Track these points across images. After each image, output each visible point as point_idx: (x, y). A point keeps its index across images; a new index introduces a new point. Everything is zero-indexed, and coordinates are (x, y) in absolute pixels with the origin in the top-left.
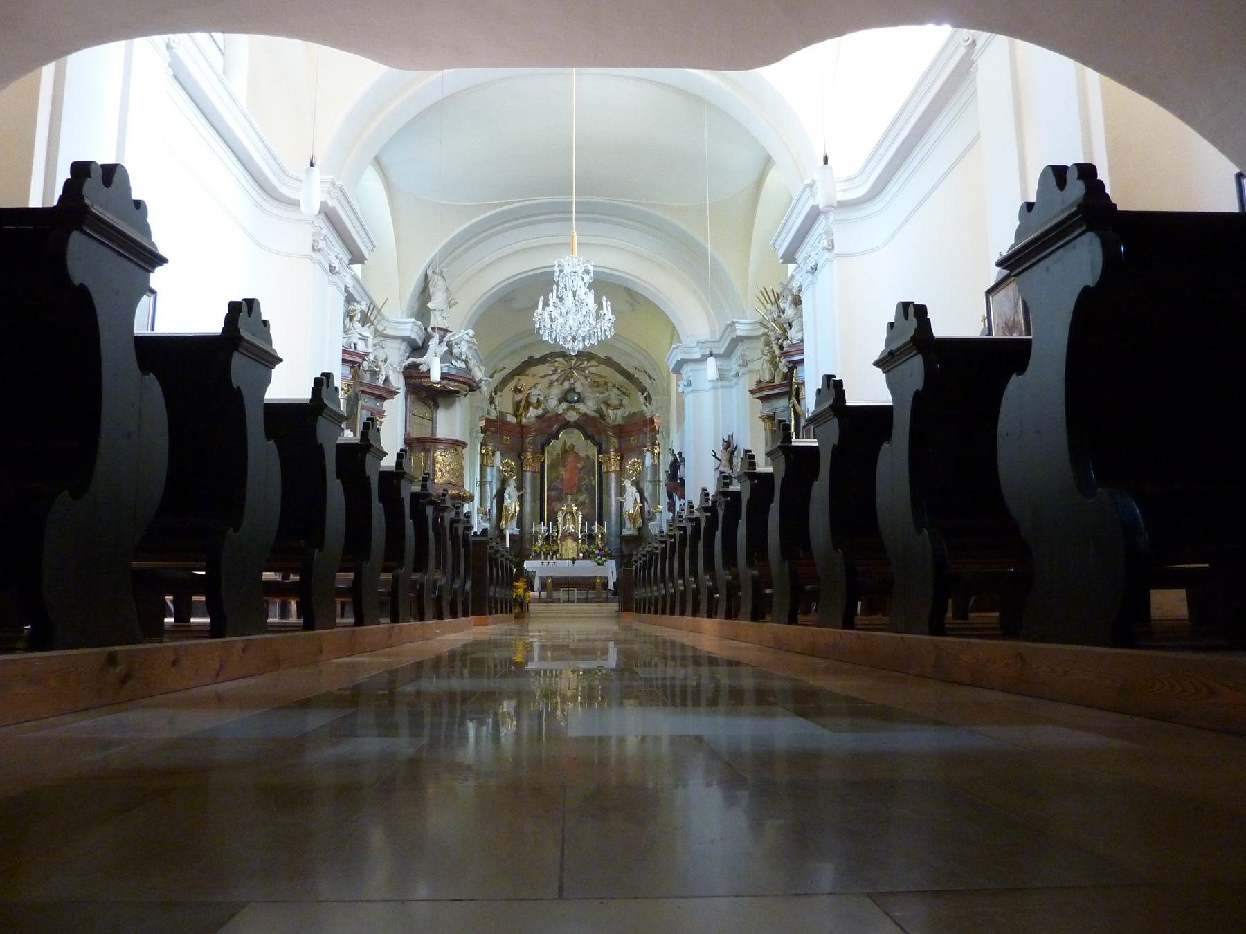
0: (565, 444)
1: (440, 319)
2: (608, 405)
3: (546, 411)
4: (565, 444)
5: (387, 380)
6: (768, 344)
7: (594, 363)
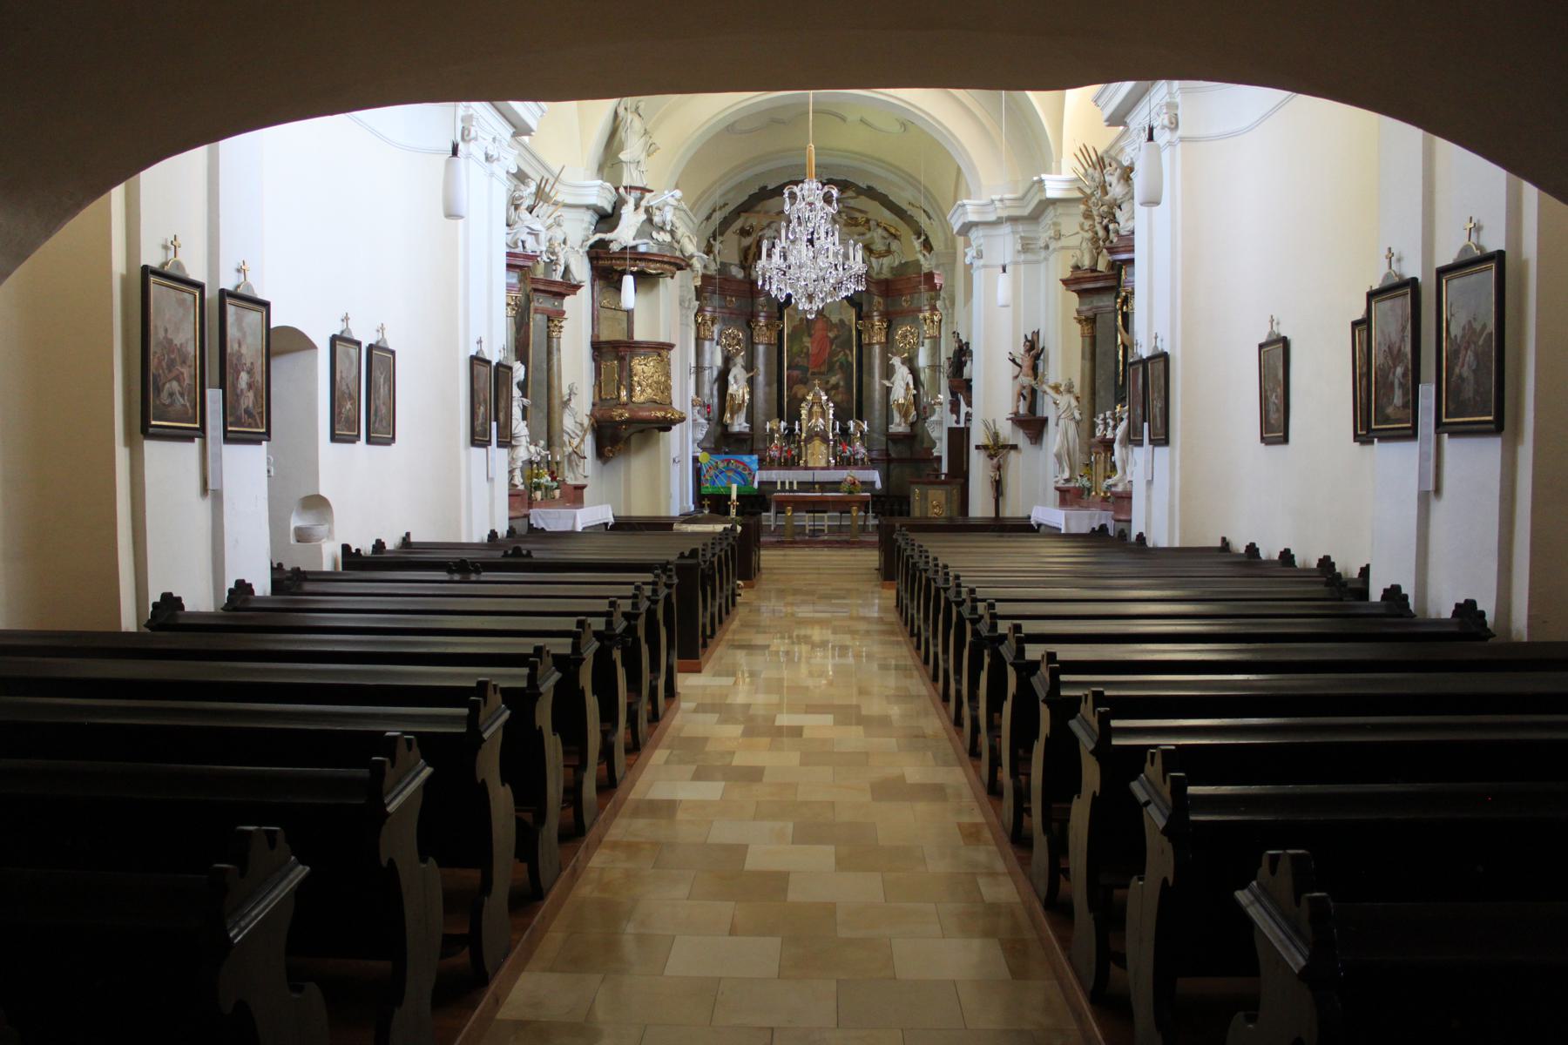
5: (567, 269)
6: (1088, 215)
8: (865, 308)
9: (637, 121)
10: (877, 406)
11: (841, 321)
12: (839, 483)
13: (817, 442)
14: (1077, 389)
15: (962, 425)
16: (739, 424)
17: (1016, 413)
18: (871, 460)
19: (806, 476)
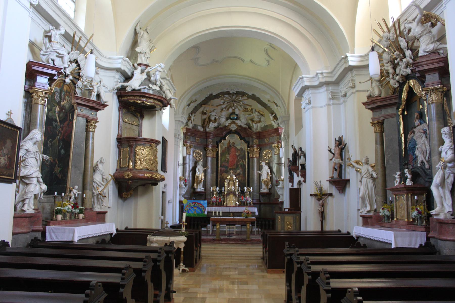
0: (229, 142)
1: (144, 58)
2: (252, 121)
3: (219, 124)
4: (229, 142)
5: (98, 96)
7: (245, 98)
8: (251, 144)
9: (146, 35)
10: (255, 182)
11: (241, 148)
12: (241, 213)
13: (231, 196)
14: (372, 161)
15: (295, 186)
16: (200, 188)
17: (332, 178)
18: (253, 203)
19: (226, 210)
